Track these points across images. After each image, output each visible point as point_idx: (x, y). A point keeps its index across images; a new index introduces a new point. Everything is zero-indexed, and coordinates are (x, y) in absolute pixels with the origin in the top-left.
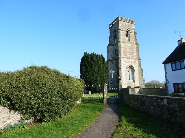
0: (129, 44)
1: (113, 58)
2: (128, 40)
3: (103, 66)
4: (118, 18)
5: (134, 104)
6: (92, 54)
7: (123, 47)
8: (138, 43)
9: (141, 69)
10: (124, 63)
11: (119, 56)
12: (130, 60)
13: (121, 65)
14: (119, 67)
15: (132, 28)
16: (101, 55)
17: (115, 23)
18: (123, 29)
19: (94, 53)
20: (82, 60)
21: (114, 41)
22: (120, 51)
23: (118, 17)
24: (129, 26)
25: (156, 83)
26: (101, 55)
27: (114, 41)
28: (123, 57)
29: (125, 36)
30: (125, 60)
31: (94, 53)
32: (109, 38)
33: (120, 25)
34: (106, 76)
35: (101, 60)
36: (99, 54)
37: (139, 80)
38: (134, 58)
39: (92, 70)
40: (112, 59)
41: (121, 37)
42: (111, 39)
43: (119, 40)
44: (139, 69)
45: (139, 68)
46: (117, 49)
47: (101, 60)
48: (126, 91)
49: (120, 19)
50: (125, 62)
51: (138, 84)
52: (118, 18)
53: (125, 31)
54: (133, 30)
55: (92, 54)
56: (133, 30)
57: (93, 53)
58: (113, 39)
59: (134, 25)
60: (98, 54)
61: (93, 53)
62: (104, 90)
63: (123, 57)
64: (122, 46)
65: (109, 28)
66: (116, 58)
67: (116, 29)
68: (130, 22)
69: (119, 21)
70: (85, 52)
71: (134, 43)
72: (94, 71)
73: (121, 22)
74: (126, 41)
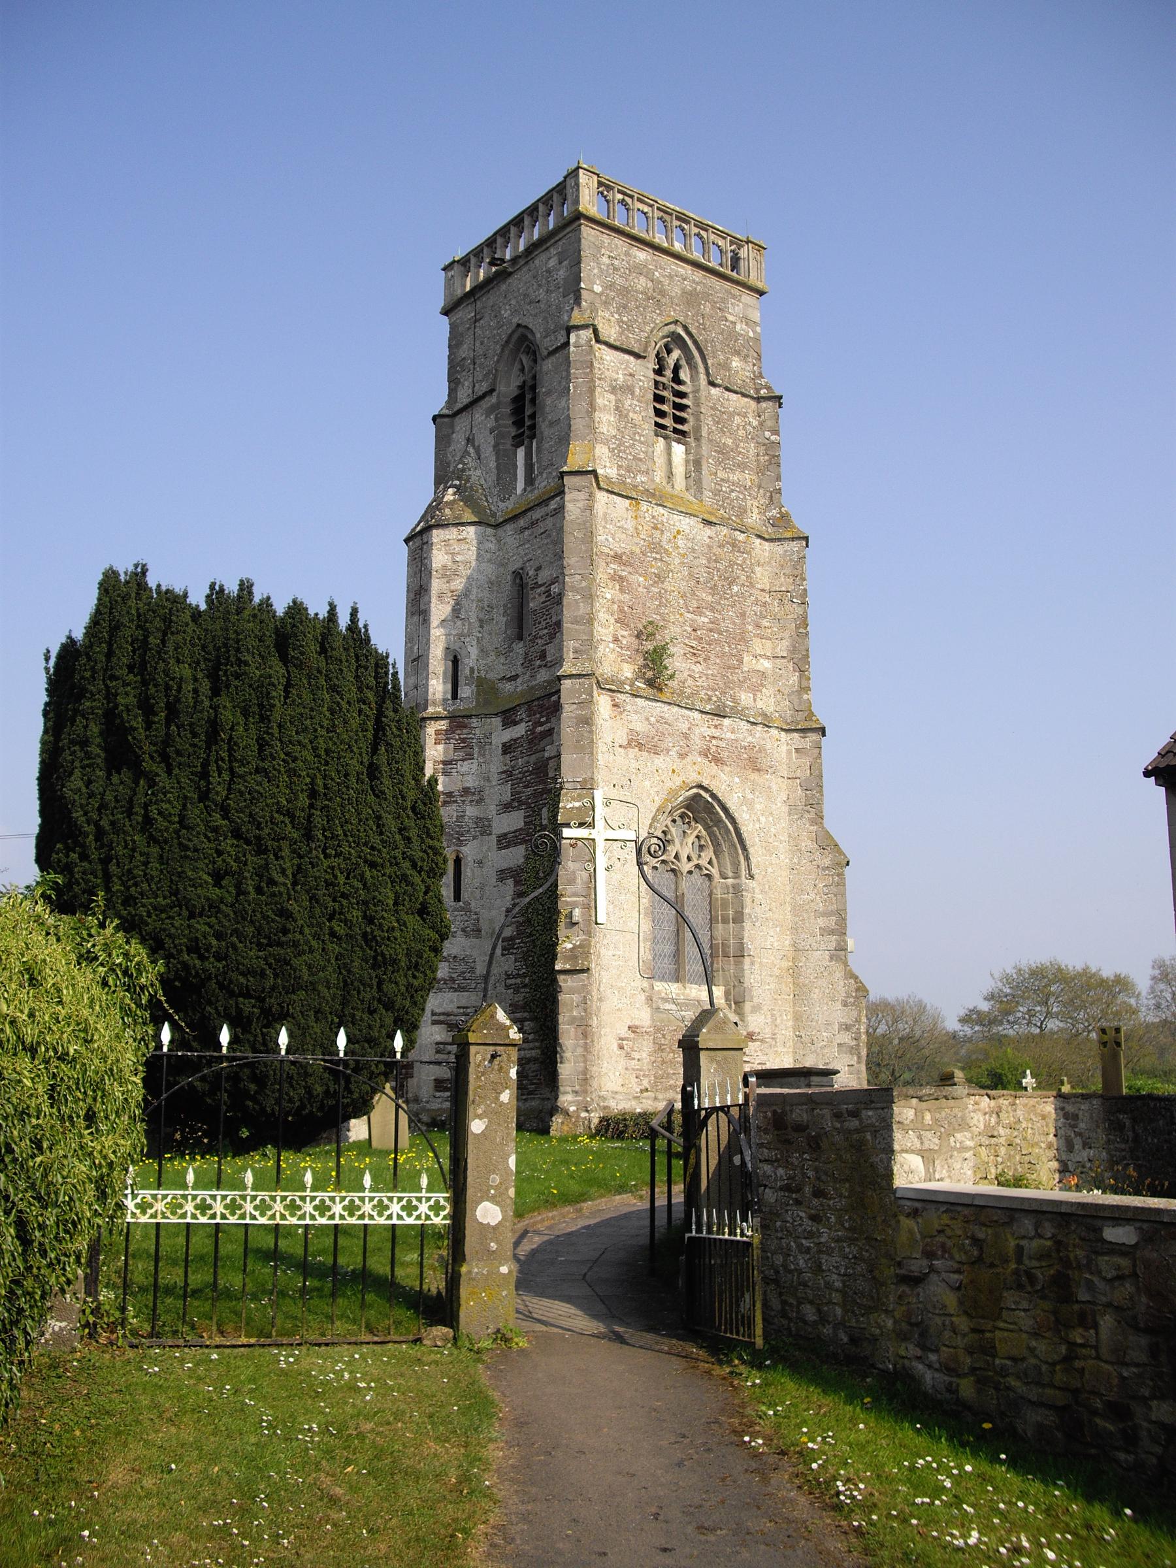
0: (686, 524)
1: (486, 688)
2: (679, 469)
3: (373, 771)
4: (564, 190)
5: (988, 1349)
6: (216, 594)
7: (617, 557)
8: (801, 524)
9: (828, 843)
10: (628, 760)
11: (567, 668)
12: (703, 727)
13: (588, 787)
14: (568, 803)
15: (732, 335)
16: (343, 621)
17: (533, 248)
18: (624, 327)
19: (246, 587)
20: (101, 584)
21: (505, 469)
22: (589, 597)
23: (574, 173)
24: (691, 298)
25: (904, 1028)
26: (343, 621)
27: (505, 469)
28: (613, 688)
29: (642, 414)
30: (640, 726)
31: (246, 587)
32: (430, 431)
33: (593, 282)
34: (413, 921)
35: (350, 690)
36: (317, 608)
37: (800, 993)
38: (745, 698)
39: (218, 820)
40: (465, 691)
41: (606, 422)
42: (459, 438)
43: (574, 461)
44: (797, 850)
45: (794, 838)
46: (545, 576)
47: (350, 690)
48: (815, 1145)
49: (589, 201)
50: (636, 742)
51: (786, 1032)
52: (564, 190)
53: (652, 364)
54: (736, 363)
55: (216, 594)
56: (736, 363)
57: (232, 588)
58: (486, 442)
59: (748, 298)
60: (297, 609)
61: (232, 588)
62: (477, 1126)
63: (613, 688)
64: (607, 539)
65: (446, 312)
66: (520, 686)
67: (537, 326)
68: (713, 264)
69: (588, 233)
70: (124, 567)
71: (754, 518)
72: (237, 834)
73: (606, 239)
74: (659, 476)
